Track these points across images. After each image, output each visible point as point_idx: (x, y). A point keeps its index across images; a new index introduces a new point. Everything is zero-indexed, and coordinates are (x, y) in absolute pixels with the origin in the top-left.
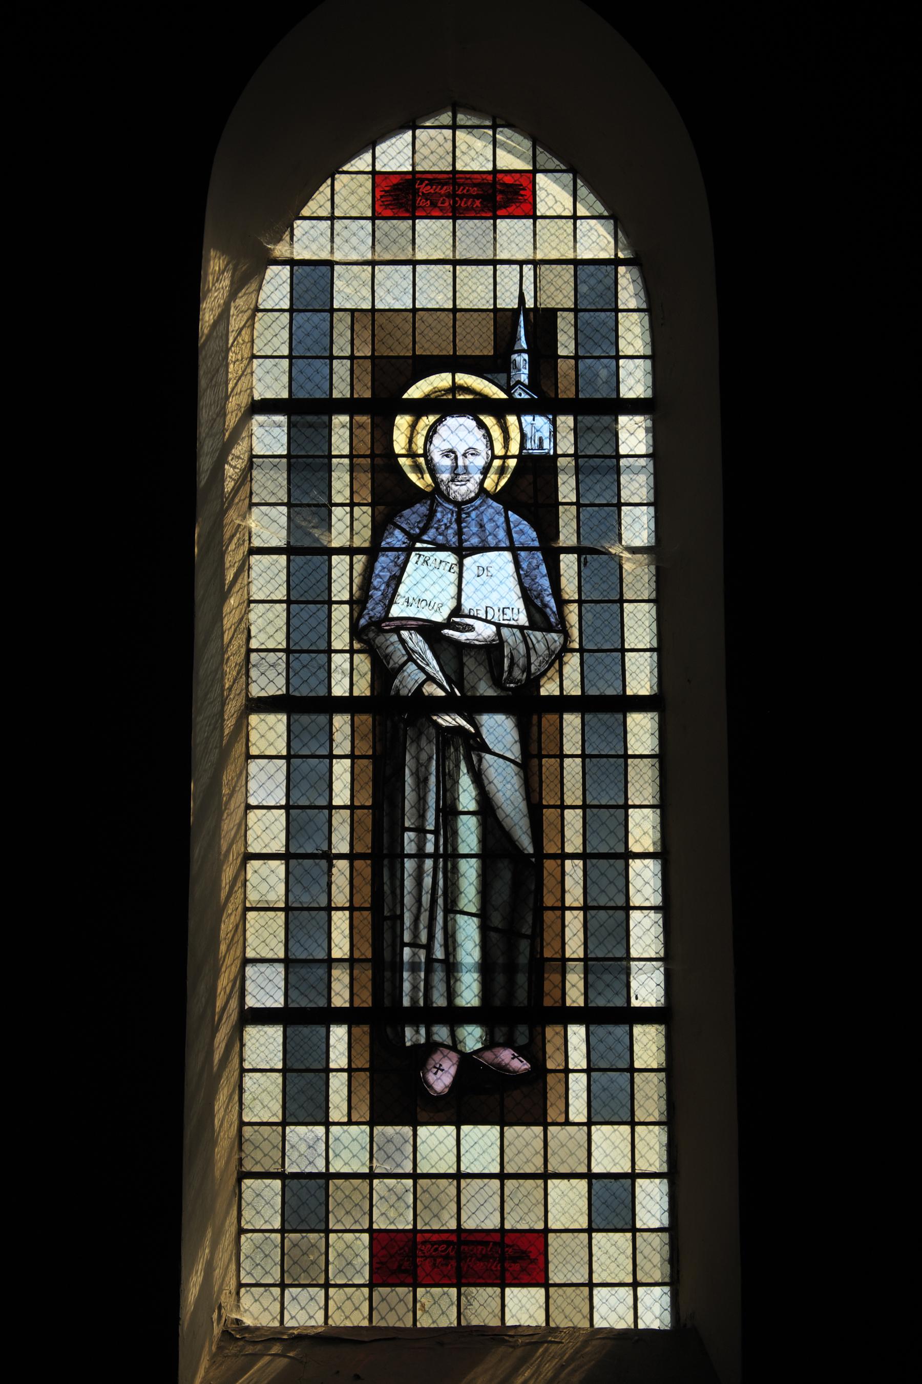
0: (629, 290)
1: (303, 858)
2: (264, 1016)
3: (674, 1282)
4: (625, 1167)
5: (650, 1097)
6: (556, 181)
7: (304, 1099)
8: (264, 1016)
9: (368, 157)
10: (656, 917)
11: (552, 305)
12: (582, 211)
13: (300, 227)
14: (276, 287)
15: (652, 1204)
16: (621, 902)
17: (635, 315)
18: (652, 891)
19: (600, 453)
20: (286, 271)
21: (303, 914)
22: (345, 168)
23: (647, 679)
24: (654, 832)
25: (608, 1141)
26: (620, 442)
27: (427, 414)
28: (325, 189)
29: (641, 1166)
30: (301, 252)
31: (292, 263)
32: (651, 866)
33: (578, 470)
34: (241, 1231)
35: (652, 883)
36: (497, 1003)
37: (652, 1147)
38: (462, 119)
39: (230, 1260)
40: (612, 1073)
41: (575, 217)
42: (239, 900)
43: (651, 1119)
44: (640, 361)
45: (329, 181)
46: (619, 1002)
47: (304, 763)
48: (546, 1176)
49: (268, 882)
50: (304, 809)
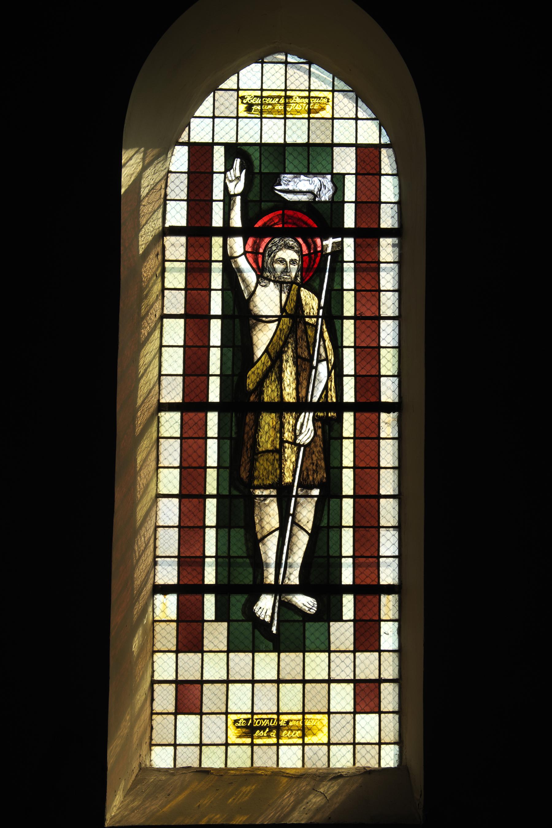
0: (387, 163)
1: (191, 495)
2: (165, 590)
3: (400, 743)
4: (374, 676)
5: (389, 636)
6: (347, 97)
7: (190, 639)
8: (165, 590)
9: (234, 78)
10: (395, 656)
11: (343, 171)
12: (360, 115)
13: (194, 122)
14: (179, 159)
15: (389, 696)
16: (376, 525)
17: (391, 715)
18: (391, 365)
19: (369, 374)
20: (186, 148)
21: (190, 528)
22: (220, 87)
23: (391, 486)
24: (394, 512)
25: (363, 462)
26: (381, 545)
27: (266, 237)
28: (210, 98)
29: (385, 676)
30: (195, 139)
31: (188, 144)
32: (392, 502)
33: (356, 270)
34: (152, 714)
35: (392, 512)
36: (301, 619)
37: (390, 669)
38: (291, 59)
39: (146, 700)
40: (366, 638)
41: (357, 119)
42: (153, 523)
43: (389, 525)
44: (392, 746)
45: (212, 93)
46: (373, 399)
47: (192, 439)
48: (329, 681)
49: (169, 512)
50: (191, 469)
